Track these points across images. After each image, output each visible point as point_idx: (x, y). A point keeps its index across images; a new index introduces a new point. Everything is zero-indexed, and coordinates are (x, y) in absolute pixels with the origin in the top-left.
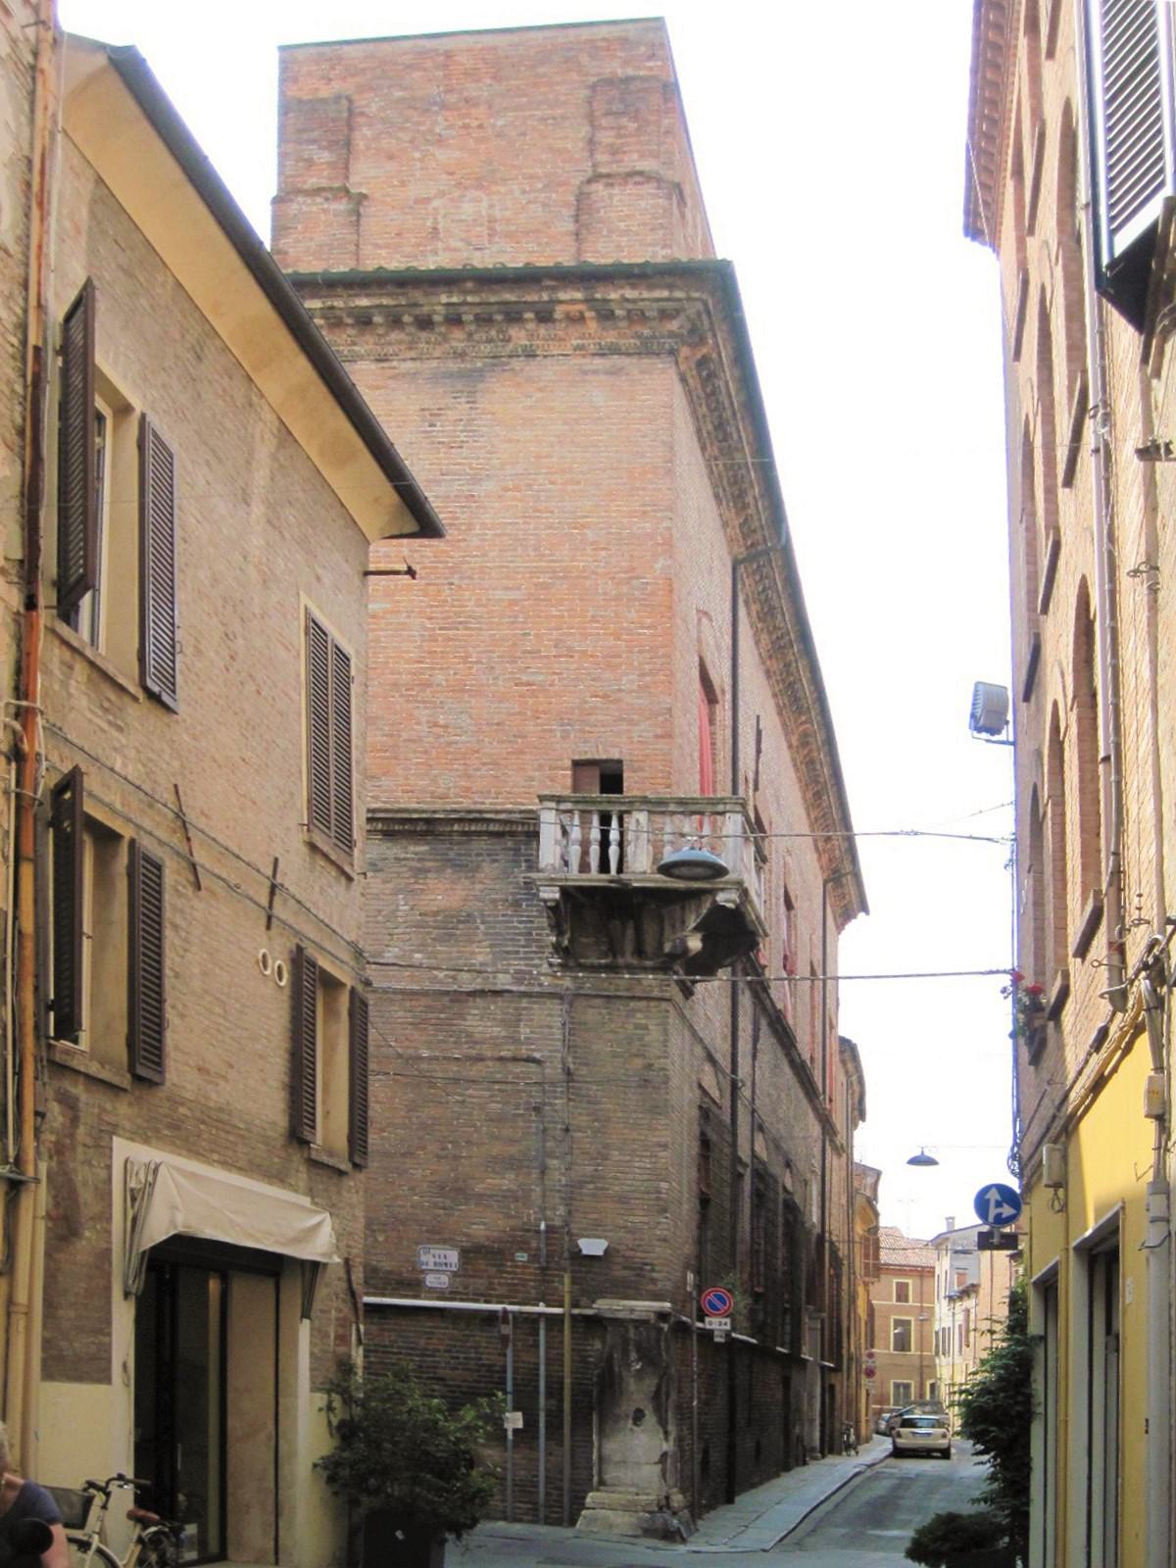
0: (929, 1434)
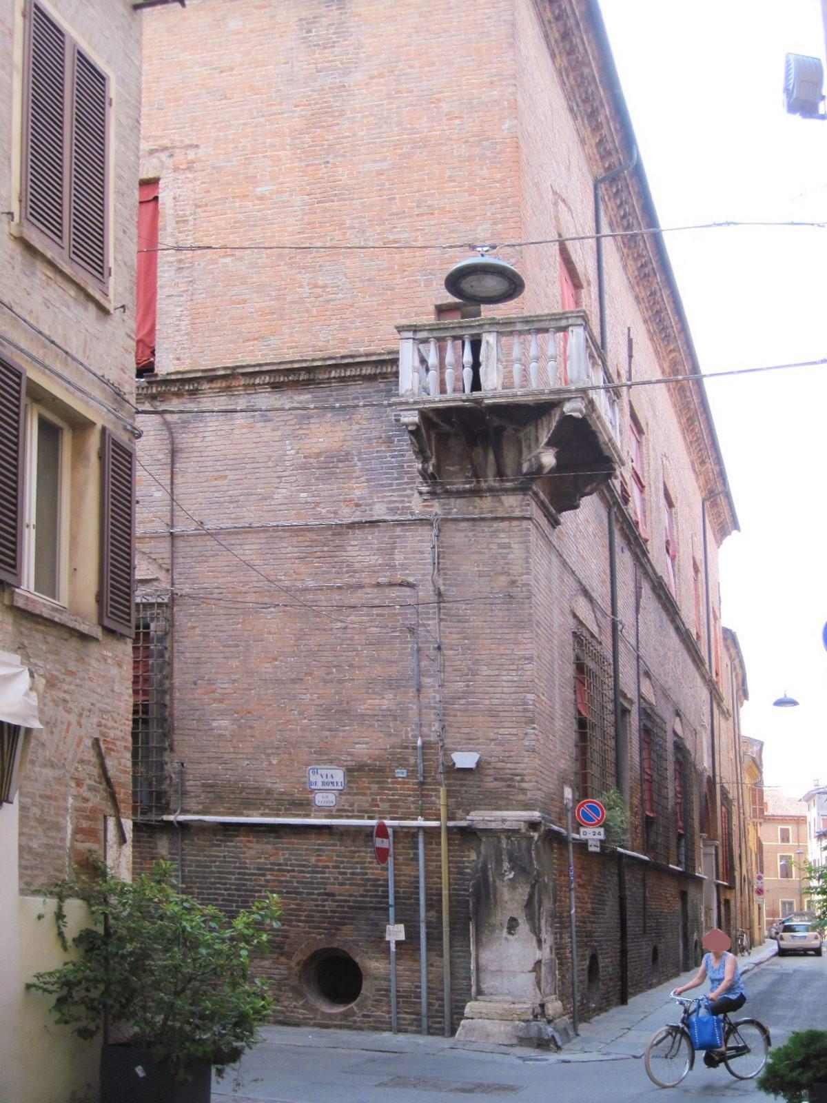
0: (805, 937)
